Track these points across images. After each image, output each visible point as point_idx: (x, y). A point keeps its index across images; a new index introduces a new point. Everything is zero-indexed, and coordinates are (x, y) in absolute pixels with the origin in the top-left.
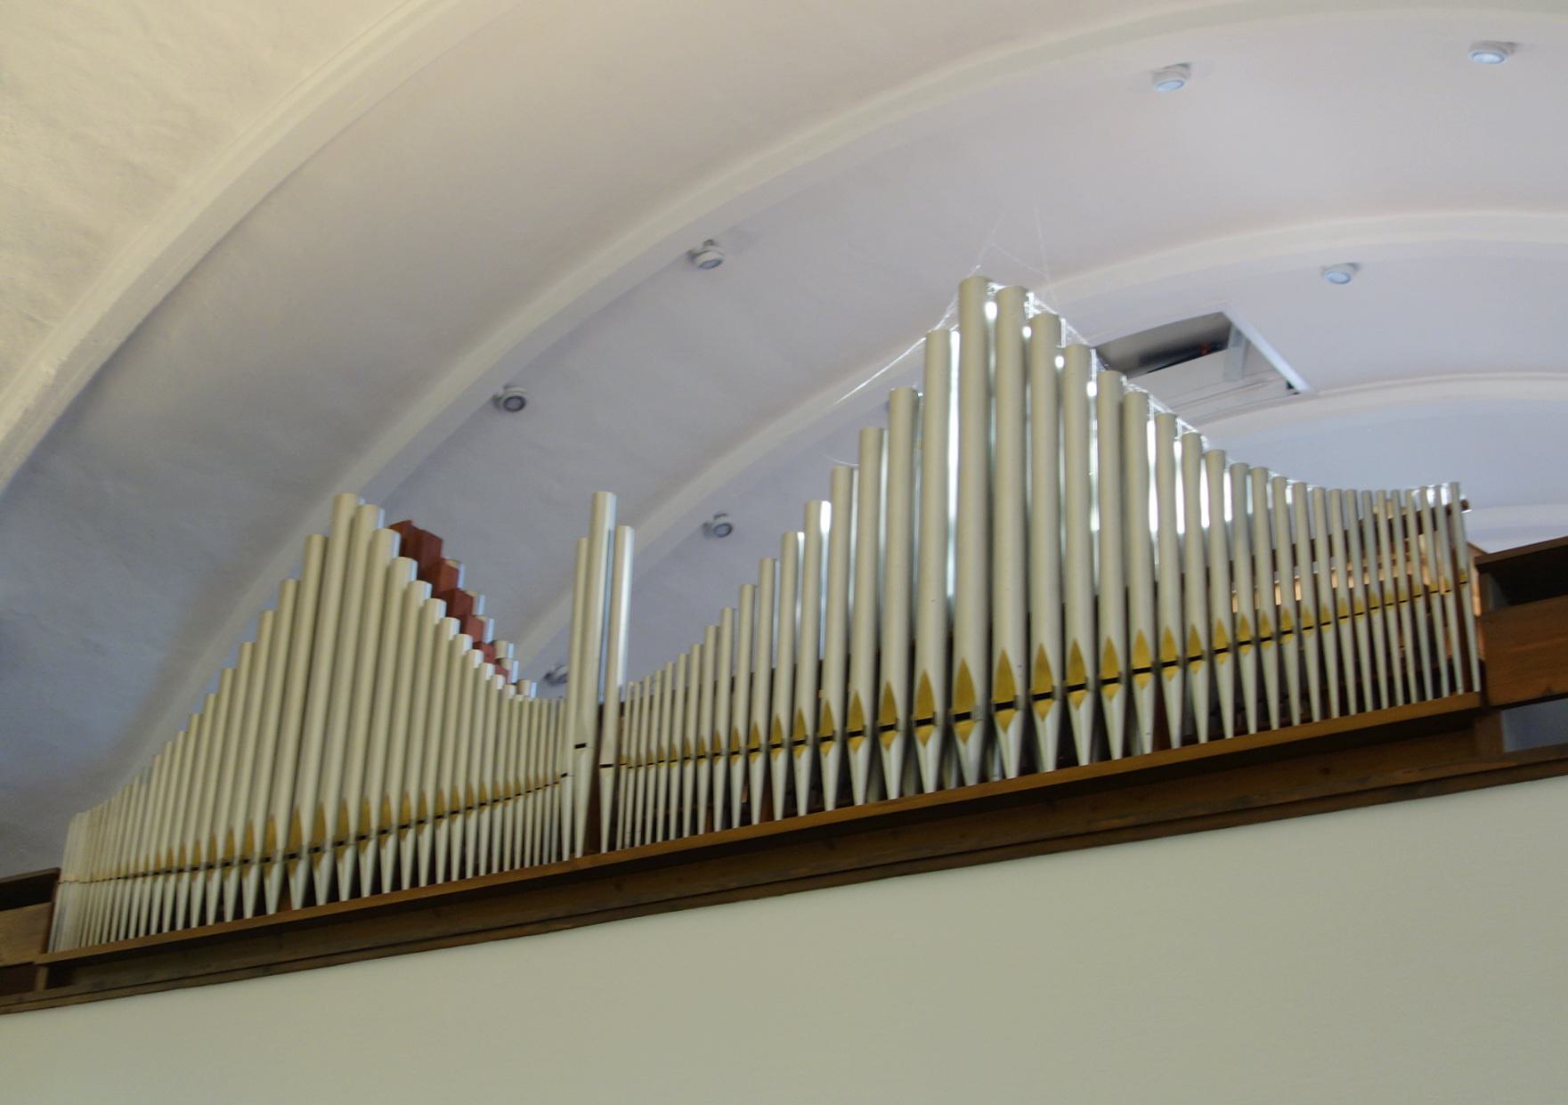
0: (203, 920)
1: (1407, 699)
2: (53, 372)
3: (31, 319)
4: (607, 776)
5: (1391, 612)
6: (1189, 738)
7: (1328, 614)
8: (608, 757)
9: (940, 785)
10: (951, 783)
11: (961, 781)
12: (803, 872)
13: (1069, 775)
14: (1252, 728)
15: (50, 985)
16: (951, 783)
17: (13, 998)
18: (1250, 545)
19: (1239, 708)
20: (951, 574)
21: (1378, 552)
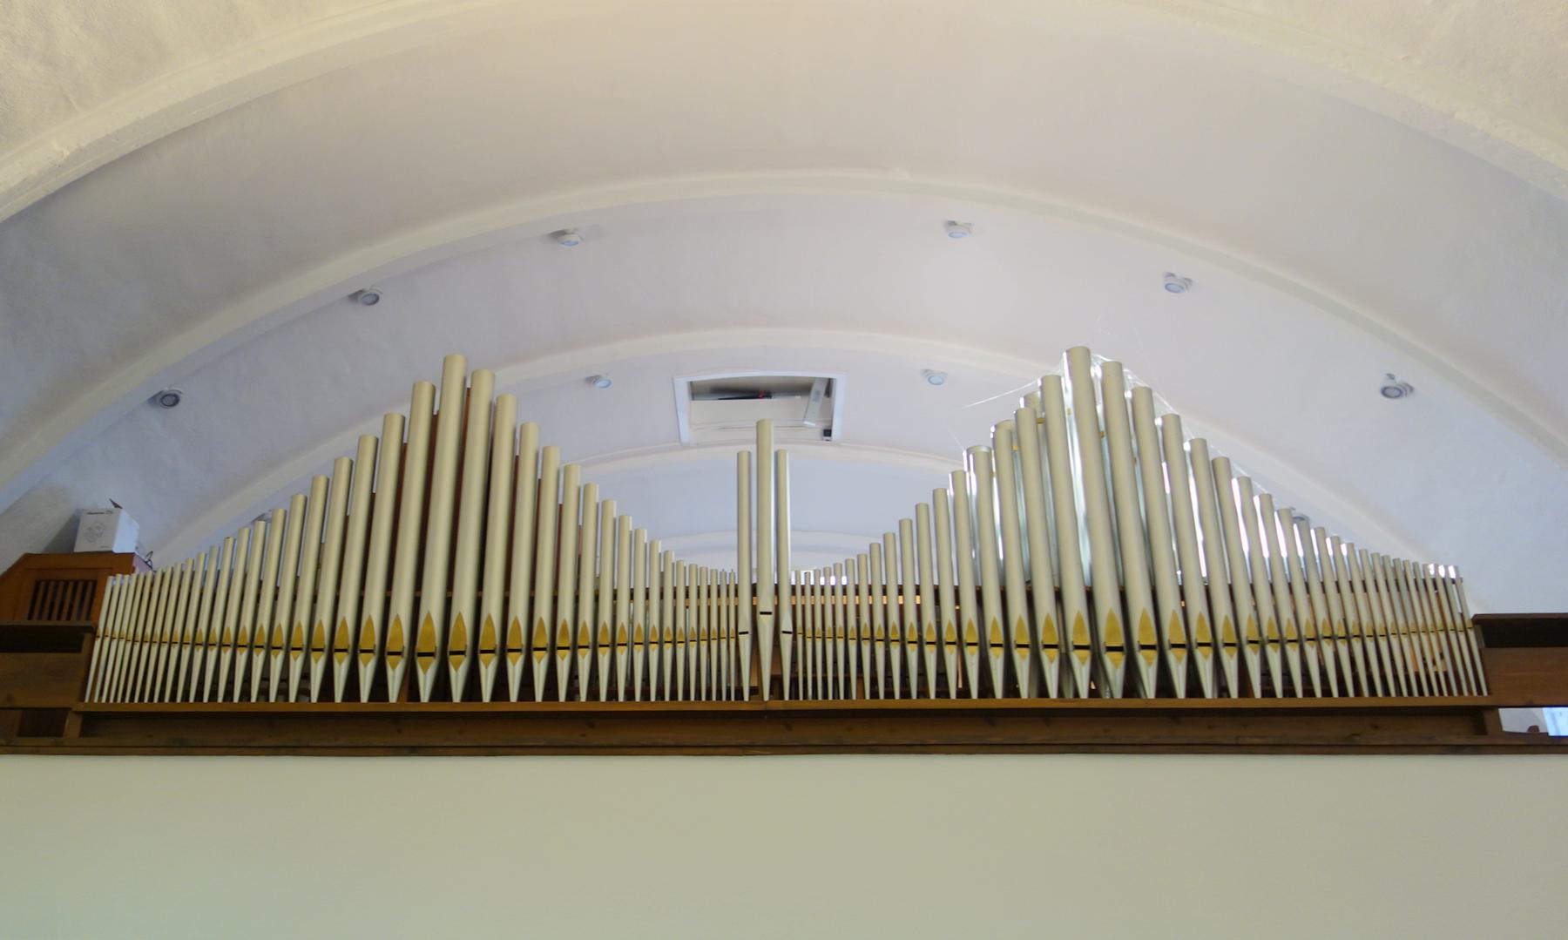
0: (264, 692)
1: (825, 696)
2: (67, 153)
3: (67, 100)
4: (786, 641)
5: (714, 644)
6: (964, 693)
7: (542, 640)
8: (786, 624)
9: (1060, 693)
10: (1069, 695)
11: (1076, 694)
12: (1037, 739)
13: (351, 707)
14: (206, 699)
15: (85, 732)
16: (1069, 695)
17: (48, 741)
18: (1309, 580)
19: (215, 683)
20: (1086, 554)
21: (709, 608)
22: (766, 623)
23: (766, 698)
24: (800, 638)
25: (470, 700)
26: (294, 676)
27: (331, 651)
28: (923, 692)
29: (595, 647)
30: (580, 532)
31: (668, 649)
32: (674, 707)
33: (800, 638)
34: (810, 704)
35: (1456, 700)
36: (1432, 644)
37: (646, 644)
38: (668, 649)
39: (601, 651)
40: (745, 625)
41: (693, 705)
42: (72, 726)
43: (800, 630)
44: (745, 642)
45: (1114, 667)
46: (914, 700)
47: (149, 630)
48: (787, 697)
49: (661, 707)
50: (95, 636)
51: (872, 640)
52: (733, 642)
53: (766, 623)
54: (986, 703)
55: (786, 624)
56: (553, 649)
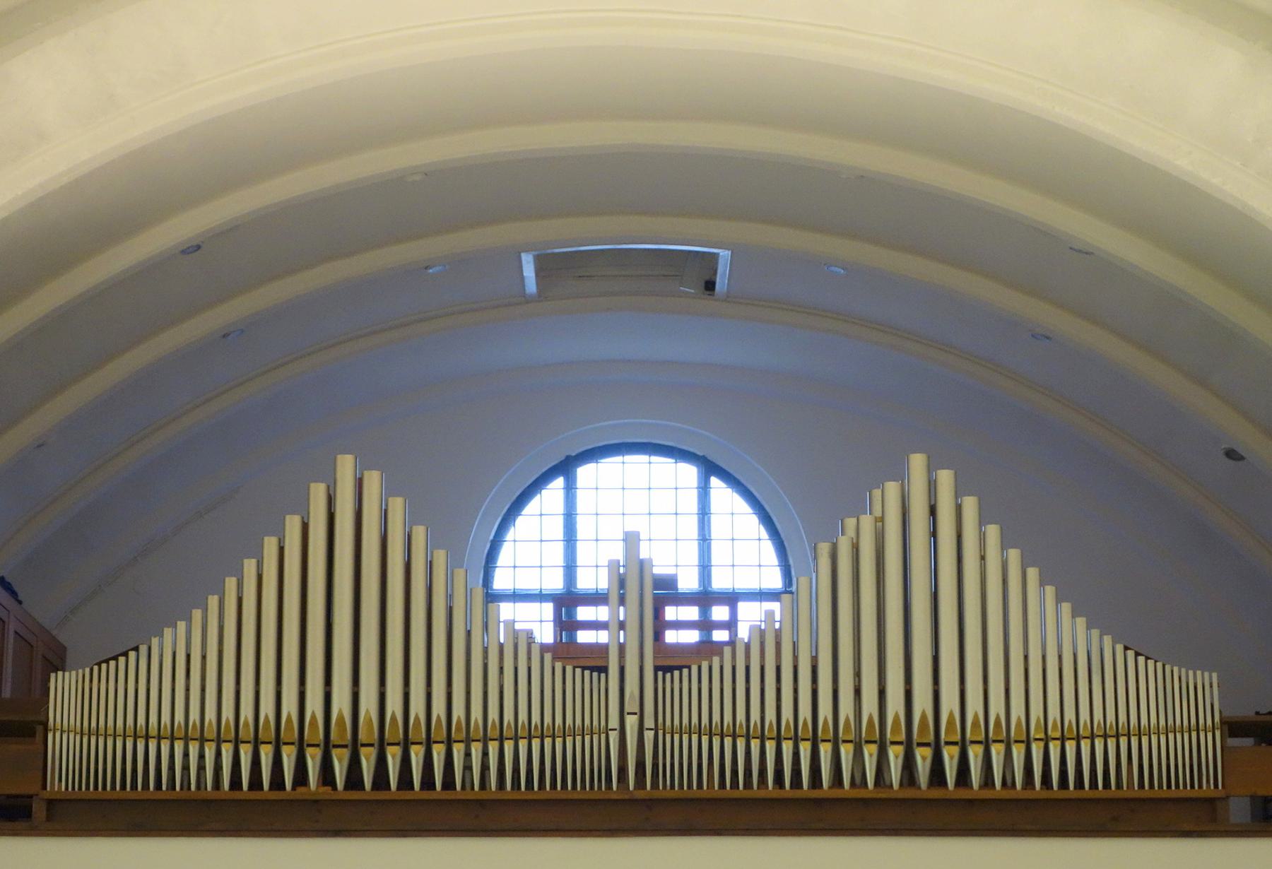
4: (649, 736)
5: (587, 738)
6: (1008, 783)
8: (649, 722)
22: (631, 721)
23: (631, 788)
24: (661, 732)
25: (352, 789)
26: (207, 765)
27: (237, 742)
28: (748, 784)
29: (1046, 741)
30: (450, 597)
31: (523, 744)
32: (554, 796)
33: (661, 732)
34: (669, 794)
35: (1196, 793)
36: (1180, 741)
37: (186, 739)
38: (1123, 741)
39: (207, 745)
40: (614, 722)
41: (1157, 793)
42: (39, 810)
43: (660, 726)
44: (614, 737)
45: (923, 758)
46: (108, 793)
47: (94, 724)
48: (523, 788)
49: (542, 796)
50: (46, 730)
51: (147, 737)
52: (603, 736)
53: (631, 721)
54: (816, 794)
55: (649, 722)
56: (449, 743)
